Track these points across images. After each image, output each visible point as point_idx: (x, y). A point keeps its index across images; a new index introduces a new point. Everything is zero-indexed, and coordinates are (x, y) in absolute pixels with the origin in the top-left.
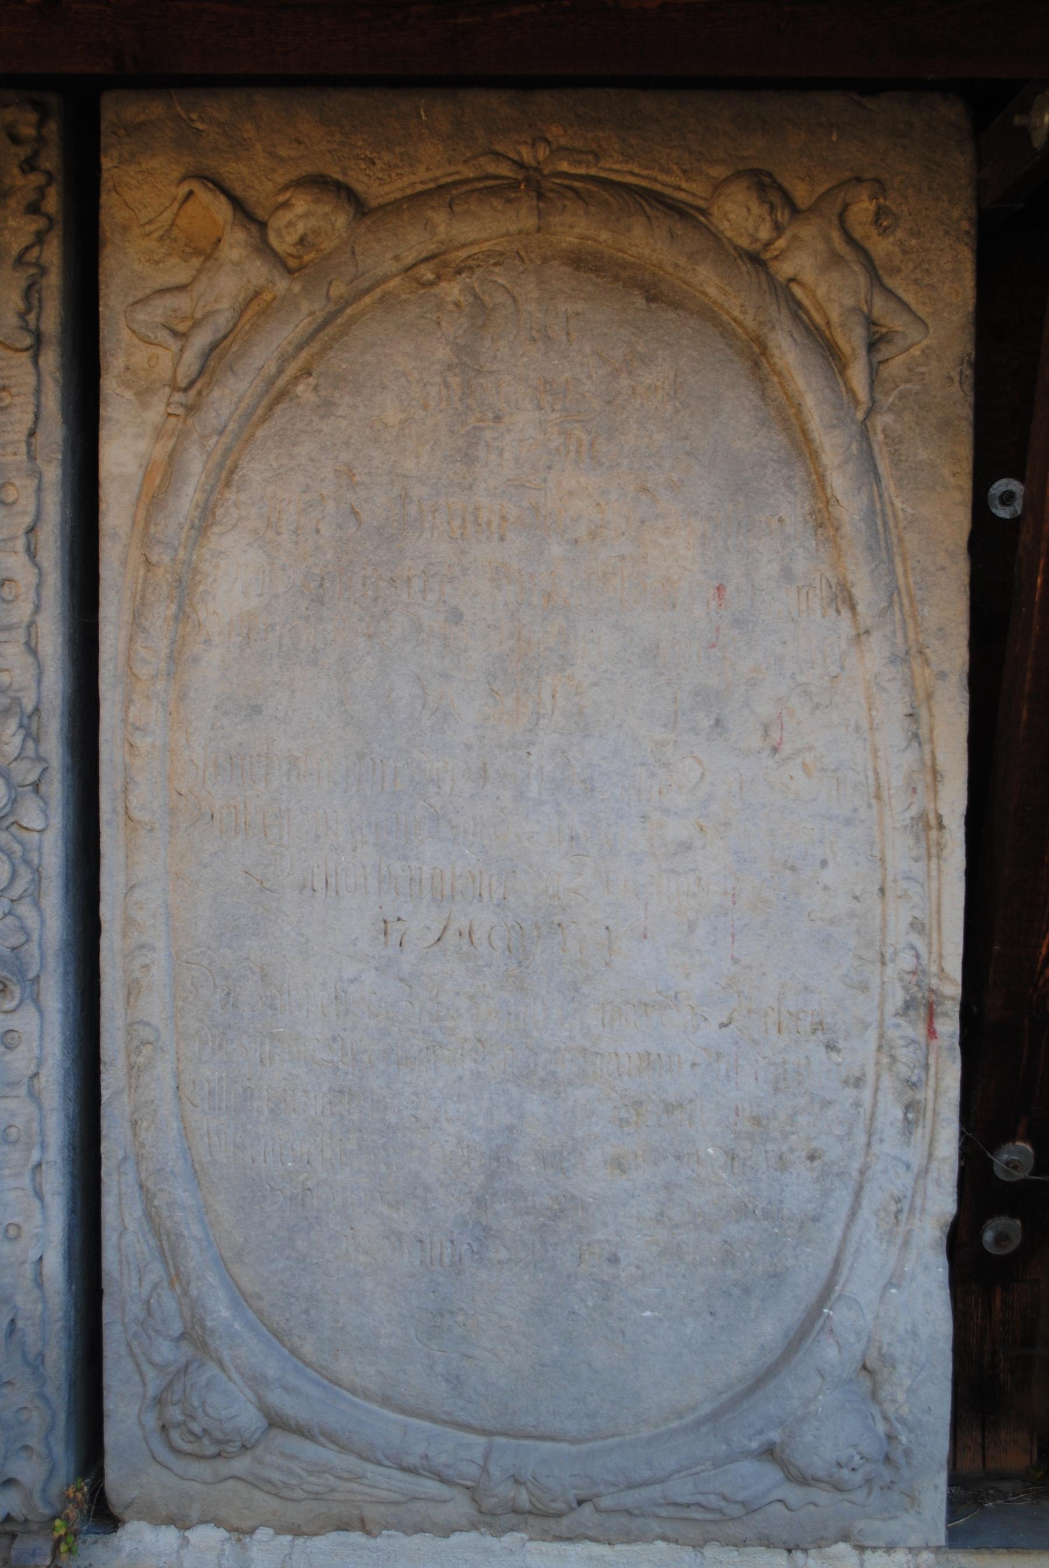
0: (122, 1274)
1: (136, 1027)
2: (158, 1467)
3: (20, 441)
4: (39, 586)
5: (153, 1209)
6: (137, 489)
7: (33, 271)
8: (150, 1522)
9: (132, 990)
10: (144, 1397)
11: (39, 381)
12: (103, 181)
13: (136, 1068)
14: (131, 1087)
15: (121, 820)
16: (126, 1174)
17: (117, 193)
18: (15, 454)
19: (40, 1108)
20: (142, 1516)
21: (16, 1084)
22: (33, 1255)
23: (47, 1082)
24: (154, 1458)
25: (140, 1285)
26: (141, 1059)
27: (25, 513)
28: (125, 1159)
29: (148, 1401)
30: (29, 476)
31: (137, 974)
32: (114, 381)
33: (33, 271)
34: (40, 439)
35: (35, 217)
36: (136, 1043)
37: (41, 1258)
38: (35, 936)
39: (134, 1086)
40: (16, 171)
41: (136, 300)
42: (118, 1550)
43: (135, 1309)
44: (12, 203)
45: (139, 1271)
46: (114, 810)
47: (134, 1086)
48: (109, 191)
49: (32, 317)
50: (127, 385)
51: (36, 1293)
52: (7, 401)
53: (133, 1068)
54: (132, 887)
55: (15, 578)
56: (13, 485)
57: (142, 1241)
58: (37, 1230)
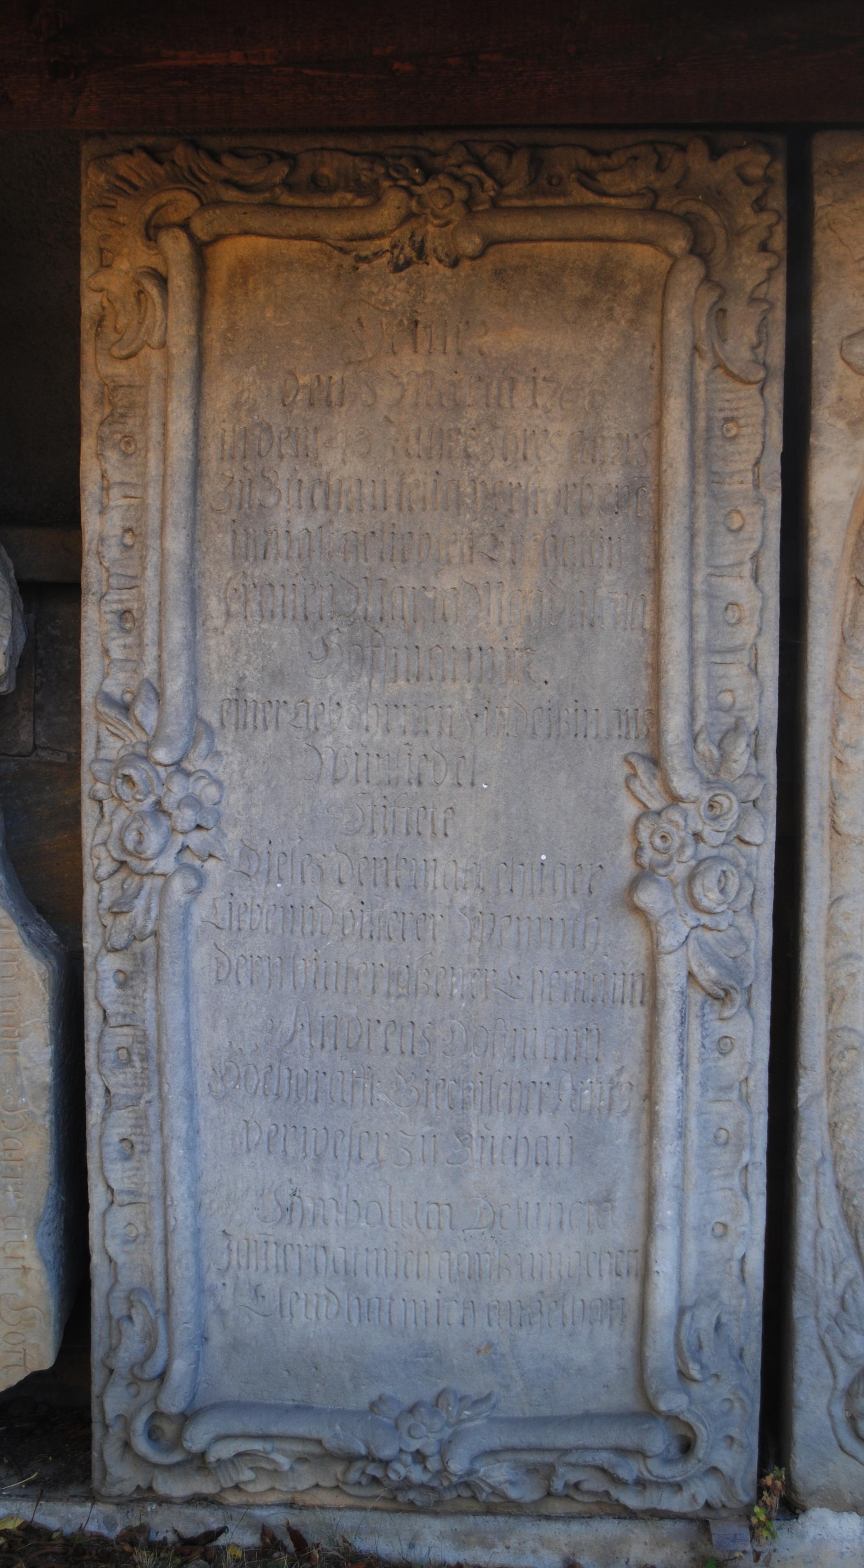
0: (816, 1270)
1: (840, 1033)
2: (844, 1456)
3: (747, 470)
4: (762, 610)
5: (851, 1208)
6: (848, 516)
7: (765, 306)
8: (832, 1509)
9: (834, 999)
10: (835, 1388)
11: (767, 413)
12: (816, 219)
13: (837, 1073)
14: (829, 1091)
15: (827, 834)
16: (824, 1174)
17: (832, 230)
18: (742, 482)
19: (750, 1112)
20: (824, 1503)
21: (730, 1088)
22: (738, 1254)
23: (755, 1086)
24: (841, 1448)
25: (834, 1281)
26: (844, 1064)
27: (751, 539)
28: (823, 1159)
29: (837, 1393)
30: (756, 503)
31: (843, 982)
32: (826, 411)
33: (765, 306)
34: (763, 468)
35: (766, 254)
36: (839, 1048)
37: (744, 1257)
38: (752, 946)
39: (834, 1089)
40: (748, 210)
41: (851, 333)
42: (802, 1536)
43: (830, 1305)
44: (746, 241)
45: (834, 1268)
46: (821, 826)
47: (834, 1089)
48: (824, 228)
49: (761, 350)
50: (840, 415)
51: (741, 1290)
52: (734, 432)
53: (833, 1072)
54: (839, 899)
55: (740, 602)
56: (738, 512)
57: (838, 1238)
58: (743, 1229)
